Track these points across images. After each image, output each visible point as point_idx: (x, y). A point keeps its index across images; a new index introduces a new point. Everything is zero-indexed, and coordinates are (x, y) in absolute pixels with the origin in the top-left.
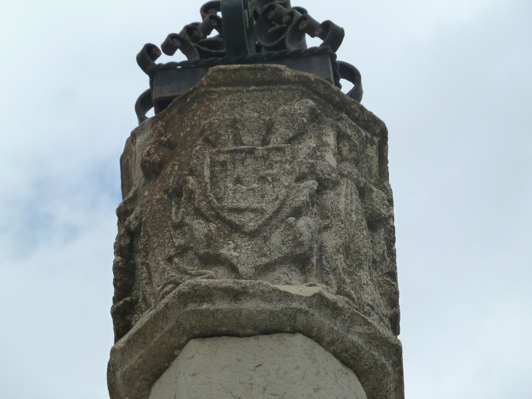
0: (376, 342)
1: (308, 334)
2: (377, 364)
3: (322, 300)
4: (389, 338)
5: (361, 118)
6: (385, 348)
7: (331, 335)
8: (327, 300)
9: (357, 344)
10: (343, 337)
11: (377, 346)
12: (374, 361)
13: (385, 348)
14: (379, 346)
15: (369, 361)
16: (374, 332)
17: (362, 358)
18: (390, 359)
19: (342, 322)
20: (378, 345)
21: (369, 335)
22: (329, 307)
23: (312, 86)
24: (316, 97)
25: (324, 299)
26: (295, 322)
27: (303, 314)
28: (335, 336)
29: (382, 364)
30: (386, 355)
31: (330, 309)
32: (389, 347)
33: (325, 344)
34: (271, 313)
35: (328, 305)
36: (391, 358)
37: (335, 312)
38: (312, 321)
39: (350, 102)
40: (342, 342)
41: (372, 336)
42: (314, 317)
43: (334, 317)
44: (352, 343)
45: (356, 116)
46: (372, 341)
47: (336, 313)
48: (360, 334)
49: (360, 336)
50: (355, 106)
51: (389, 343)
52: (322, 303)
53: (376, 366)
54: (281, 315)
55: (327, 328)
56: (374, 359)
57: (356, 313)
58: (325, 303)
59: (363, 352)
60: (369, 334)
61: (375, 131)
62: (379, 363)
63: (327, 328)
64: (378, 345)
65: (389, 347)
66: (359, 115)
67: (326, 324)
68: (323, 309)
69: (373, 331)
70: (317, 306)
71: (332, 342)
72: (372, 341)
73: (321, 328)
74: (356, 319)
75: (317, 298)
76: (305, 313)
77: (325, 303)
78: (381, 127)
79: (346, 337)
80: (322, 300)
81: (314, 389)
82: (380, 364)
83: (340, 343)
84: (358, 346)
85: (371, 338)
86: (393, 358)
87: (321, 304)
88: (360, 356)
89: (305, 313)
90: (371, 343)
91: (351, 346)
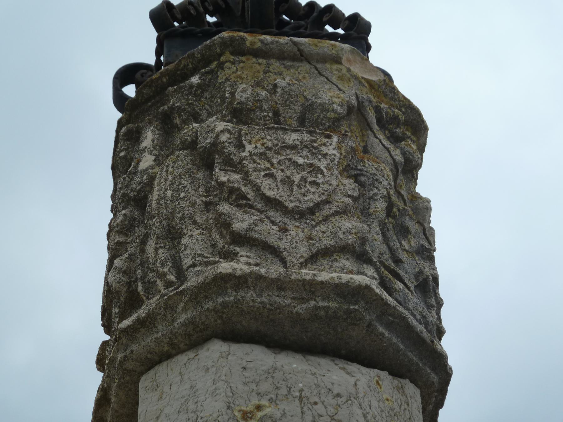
0: (202, 296)
1: (154, 363)
2: (218, 311)
3: (127, 332)
4: (205, 280)
5: (196, 63)
6: (213, 290)
7: (163, 344)
8: (129, 327)
9: (187, 322)
10: (171, 333)
11: (206, 297)
12: (213, 312)
13: (213, 290)
14: (207, 294)
15: (210, 317)
16: (191, 292)
17: (203, 323)
18: (226, 291)
19: (163, 320)
20: (205, 296)
21: (190, 300)
22: (138, 328)
23: (140, 101)
24: (149, 104)
25: (127, 330)
26: (135, 371)
27: (125, 362)
28: (165, 340)
29: (221, 305)
30: (220, 292)
31: (141, 328)
32: (215, 285)
33: (173, 352)
34: (120, 388)
35: (135, 328)
36: (226, 288)
37: (148, 323)
38: (138, 356)
39: (177, 66)
40: (176, 336)
41: (193, 297)
42: (134, 352)
43: (152, 328)
44: (183, 325)
45: (191, 68)
46: (198, 300)
47: (150, 324)
48: (185, 309)
49: (186, 310)
50: (183, 63)
51: (209, 283)
52: (130, 334)
53: (220, 313)
54: (122, 381)
55: (153, 345)
56: (211, 311)
57: (167, 298)
58: (132, 331)
59: (197, 320)
60: (189, 300)
61: (217, 53)
62: (219, 307)
63: (153, 345)
64: (205, 296)
65: (215, 285)
66: (192, 64)
67: (148, 343)
68: (137, 335)
69: (189, 292)
70: (131, 340)
71: (172, 344)
72: (198, 300)
73: (150, 351)
74: (172, 302)
75: (124, 336)
76: (125, 360)
77: (132, 331)
78: (217, 44)
79: (174, 328)
80: (127, 332)
81: (277, 369)
82: (220, 308)
83: (176, 338)
84: (189, 321)
85: (195, 299)
86: (229, 286)
87: (131, 335)
88: (201, 324)
89: (125, 360)
90: (200, 302)
91: (185, 328)
